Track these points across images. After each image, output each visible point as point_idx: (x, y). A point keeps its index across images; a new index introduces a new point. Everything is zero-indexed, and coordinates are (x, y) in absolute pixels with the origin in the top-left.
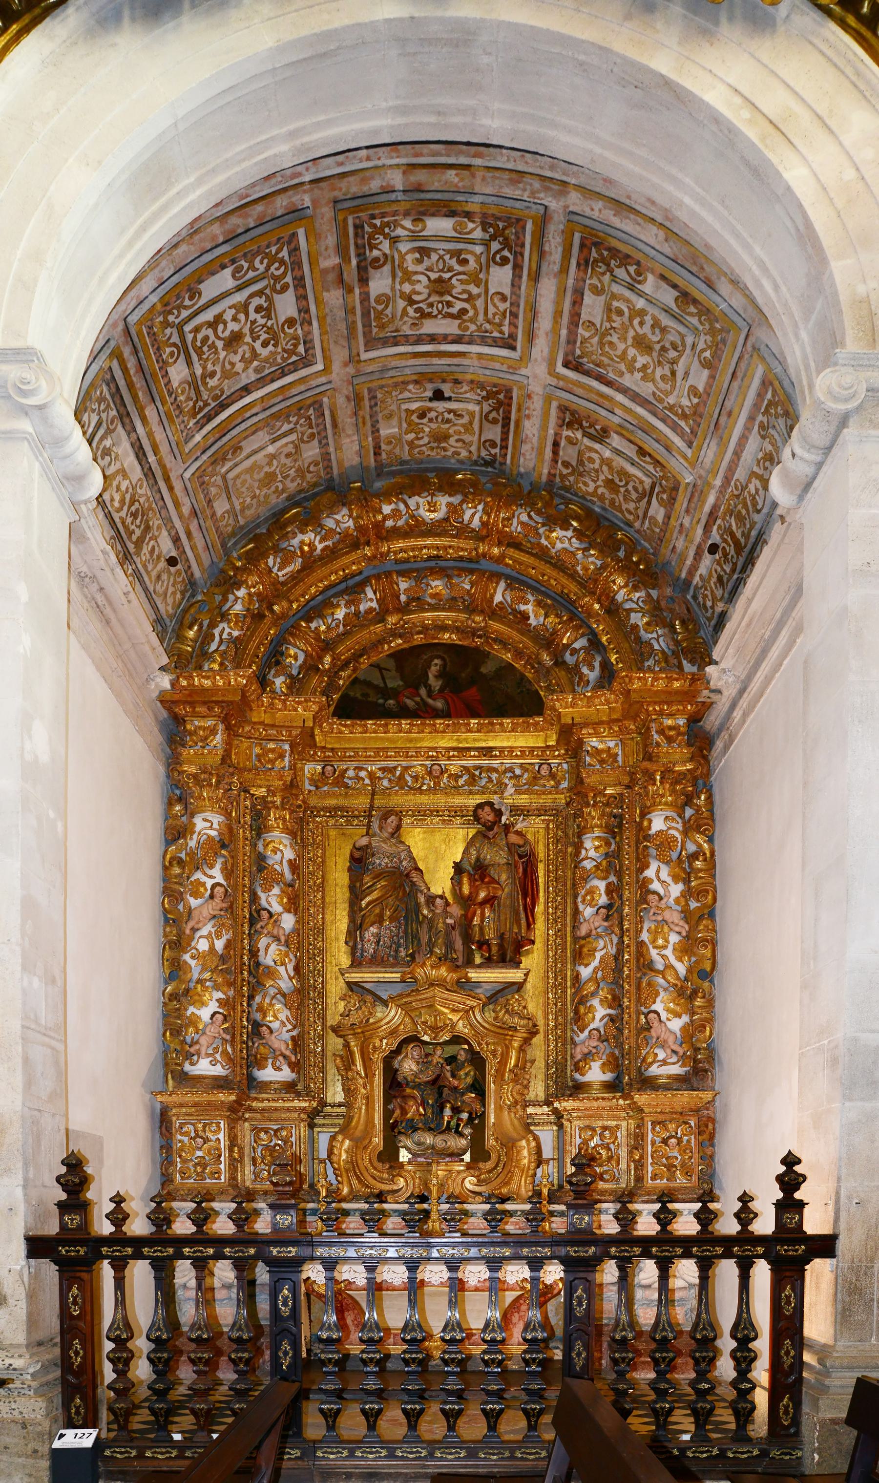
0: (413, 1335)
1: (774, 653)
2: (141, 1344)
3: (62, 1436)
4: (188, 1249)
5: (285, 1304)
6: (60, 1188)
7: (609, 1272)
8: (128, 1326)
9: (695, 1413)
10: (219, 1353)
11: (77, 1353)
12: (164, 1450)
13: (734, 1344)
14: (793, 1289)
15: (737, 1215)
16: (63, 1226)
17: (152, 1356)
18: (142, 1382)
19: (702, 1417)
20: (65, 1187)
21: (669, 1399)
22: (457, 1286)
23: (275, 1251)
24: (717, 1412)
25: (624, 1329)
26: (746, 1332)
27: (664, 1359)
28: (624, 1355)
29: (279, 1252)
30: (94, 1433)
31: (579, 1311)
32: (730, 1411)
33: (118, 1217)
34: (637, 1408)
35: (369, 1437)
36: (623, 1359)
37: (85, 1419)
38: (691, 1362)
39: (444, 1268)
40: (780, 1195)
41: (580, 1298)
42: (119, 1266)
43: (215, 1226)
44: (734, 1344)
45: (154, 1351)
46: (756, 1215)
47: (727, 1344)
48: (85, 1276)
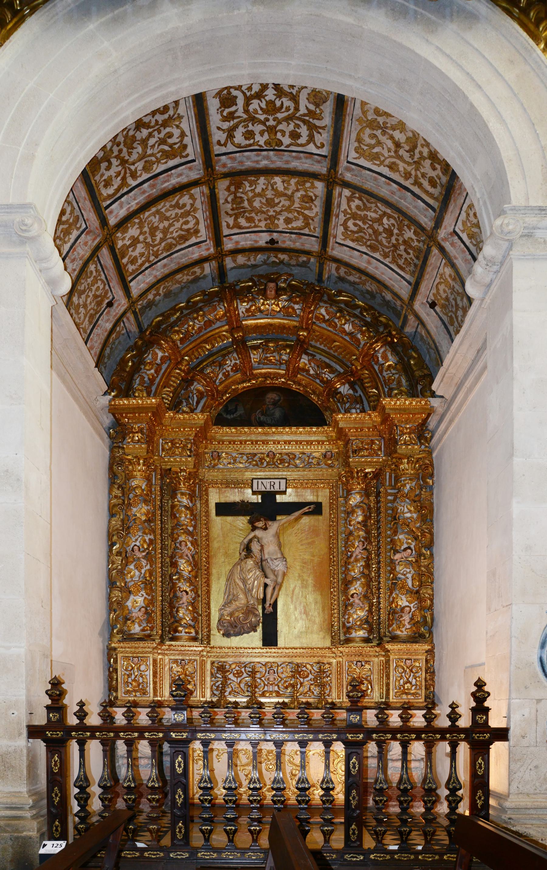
0: (278, 785)
1: (468, 384)
2: (95, 790)
4: (147, 734)
6: (47, 697)
7: (372, 748)
8: (86, 779)
9: (425, 834)
10: (141, 796)
11: (180, 796)
13: (447, 792)
14: (483, 759)
15: (449, 716)
16: (49, 719)
17: (101, 796)
18: (95, 812)
19: (428, 836)
20: (50, 696)
21: (409, 825)
22: (256, 756)
24: (437, 833)
25: (381, 783)
26: (153, 784)
28: (381, 798)
29: (352, 737)
30: (63, 844)
31: (354, 772)
32: (446, 833)
33: (454, 716)
34: (389, 830)
35: (254, 846)
36: (381, 801)
37: (61, 833)
38: (422, 803)
40: (473, 704)
42: (82, 743)
43: (90, 721)
44: (447, 792)
45: (102, 794)
46: (460, 716)
47: (444, 792)
48: (359, 751)
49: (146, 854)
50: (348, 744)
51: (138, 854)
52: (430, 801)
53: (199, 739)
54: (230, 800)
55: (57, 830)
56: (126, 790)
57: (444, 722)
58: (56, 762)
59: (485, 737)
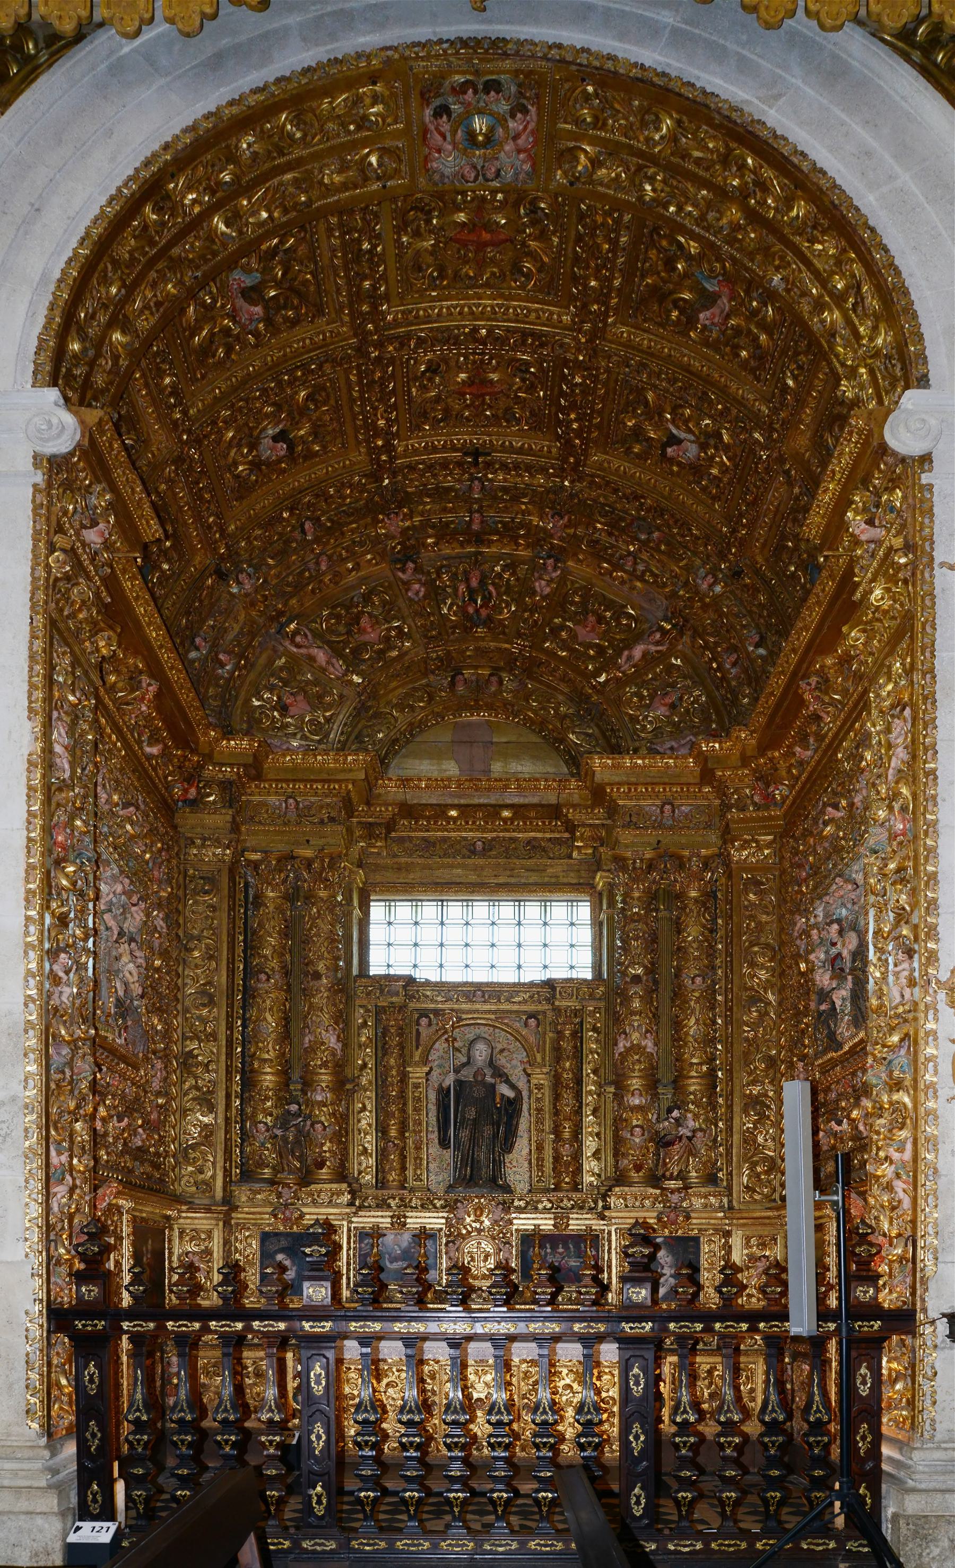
3: (78, 1529)
27: (818, 1443)
30: (113, 1527)
39: (399, 1344)
41: (636, 1377)
53: (127, 1332)
54: (545, 1444)
55: (95, 1501)
57: (710, 1298)
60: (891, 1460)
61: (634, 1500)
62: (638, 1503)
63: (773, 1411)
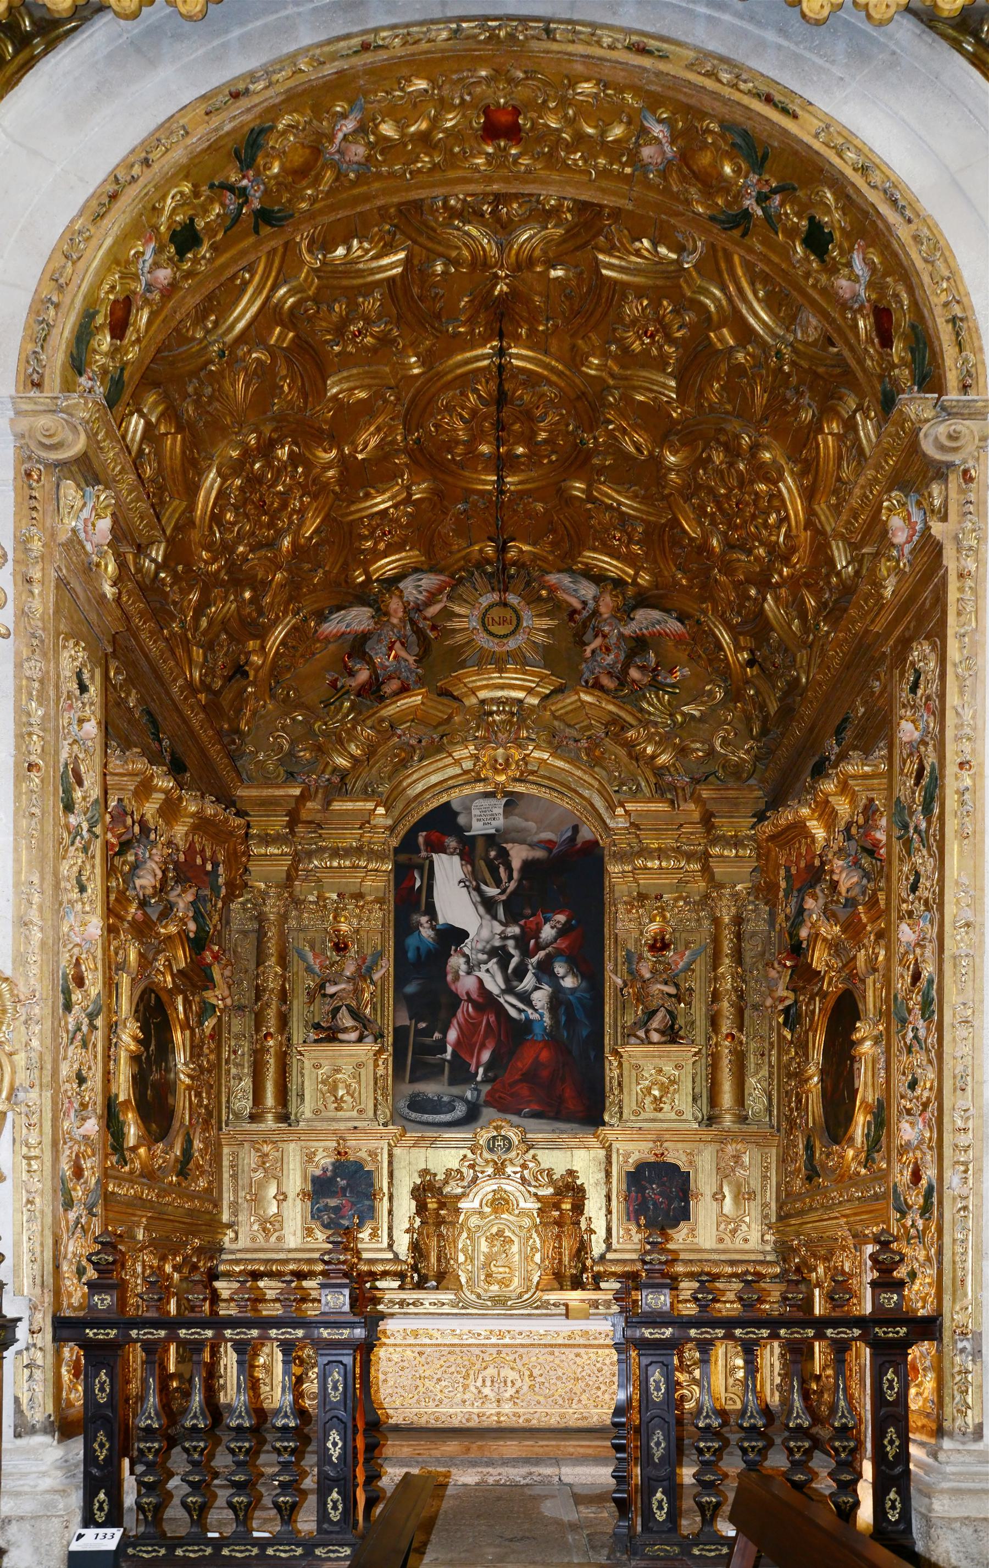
4: (184, 1331)
5: (335, 1388)
11: (335, 1444)
12: (287, 1548)
23: (90, 1333)
30: (118, 1532)
42: (246, 1351)
48: (899, 1359)
49: (270, 1552)
50: (878, 1346)
51: (255, 1551)
52: (844, 1448)
53: (231, 1340)
55: (101, 1509)
56: (141, 1434)
58: (102, 1384)
59: (898, 1333)
60: (920, 1465)
61: (889, 1504)
62: (660, 1508)
63: (798, 1416)
